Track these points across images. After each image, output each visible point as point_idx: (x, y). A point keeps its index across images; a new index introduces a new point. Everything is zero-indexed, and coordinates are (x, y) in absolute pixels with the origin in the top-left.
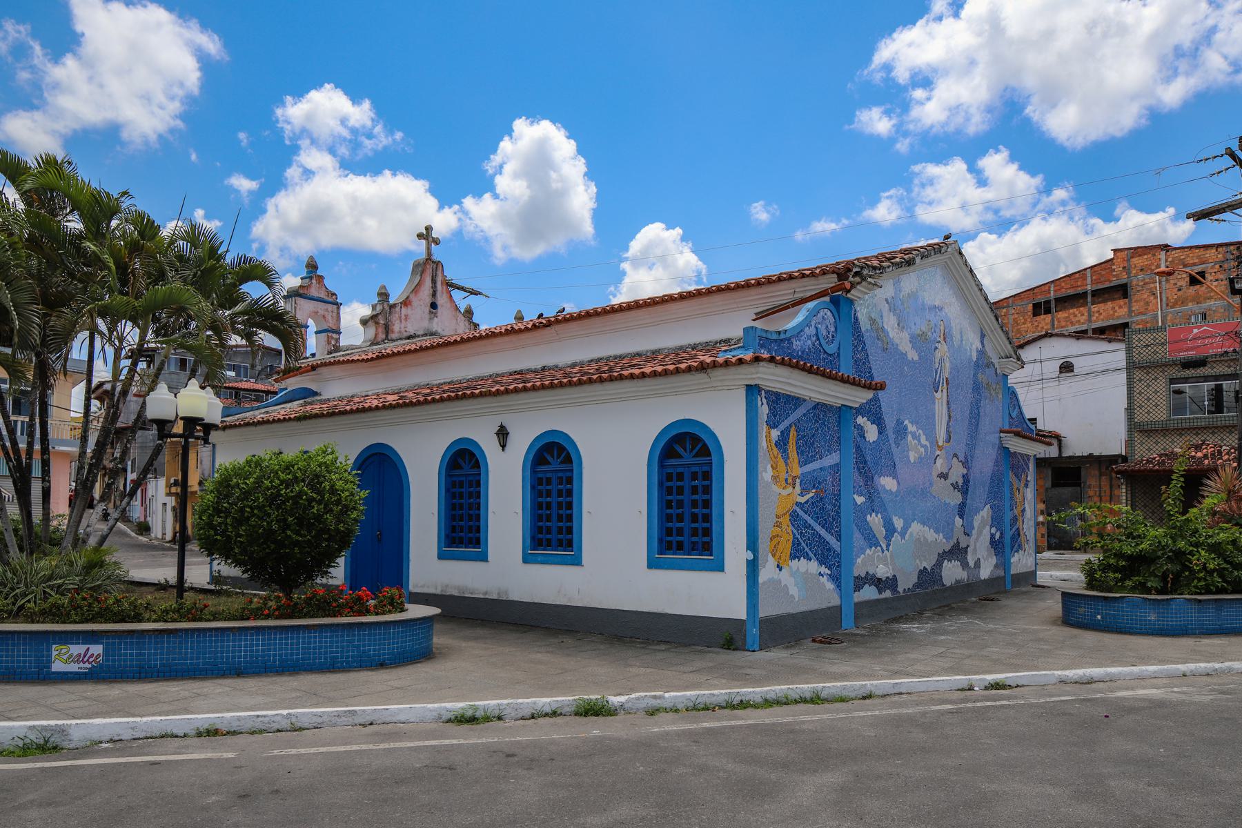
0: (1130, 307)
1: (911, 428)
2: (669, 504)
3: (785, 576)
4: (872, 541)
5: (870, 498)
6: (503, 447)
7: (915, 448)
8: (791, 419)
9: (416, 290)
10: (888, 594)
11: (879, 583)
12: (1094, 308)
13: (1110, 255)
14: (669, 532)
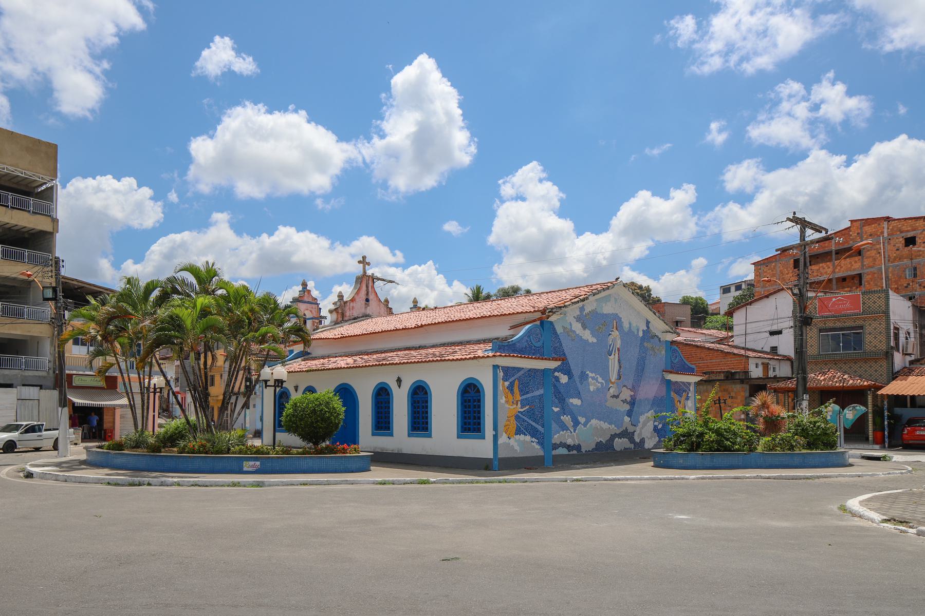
0: (862, 263)
1: (590, 375)
2: (465, 412)
3: (512, 442)
4: (564, 427)
5: (563, 409)
6: (399, 387)
7: (594, 383)
8: (516, 377)
9: (357, 293)
10: (575, 452)
11: (569, 447)
12: (837, 262)
13: (849, 224)
14: (465, 424)
